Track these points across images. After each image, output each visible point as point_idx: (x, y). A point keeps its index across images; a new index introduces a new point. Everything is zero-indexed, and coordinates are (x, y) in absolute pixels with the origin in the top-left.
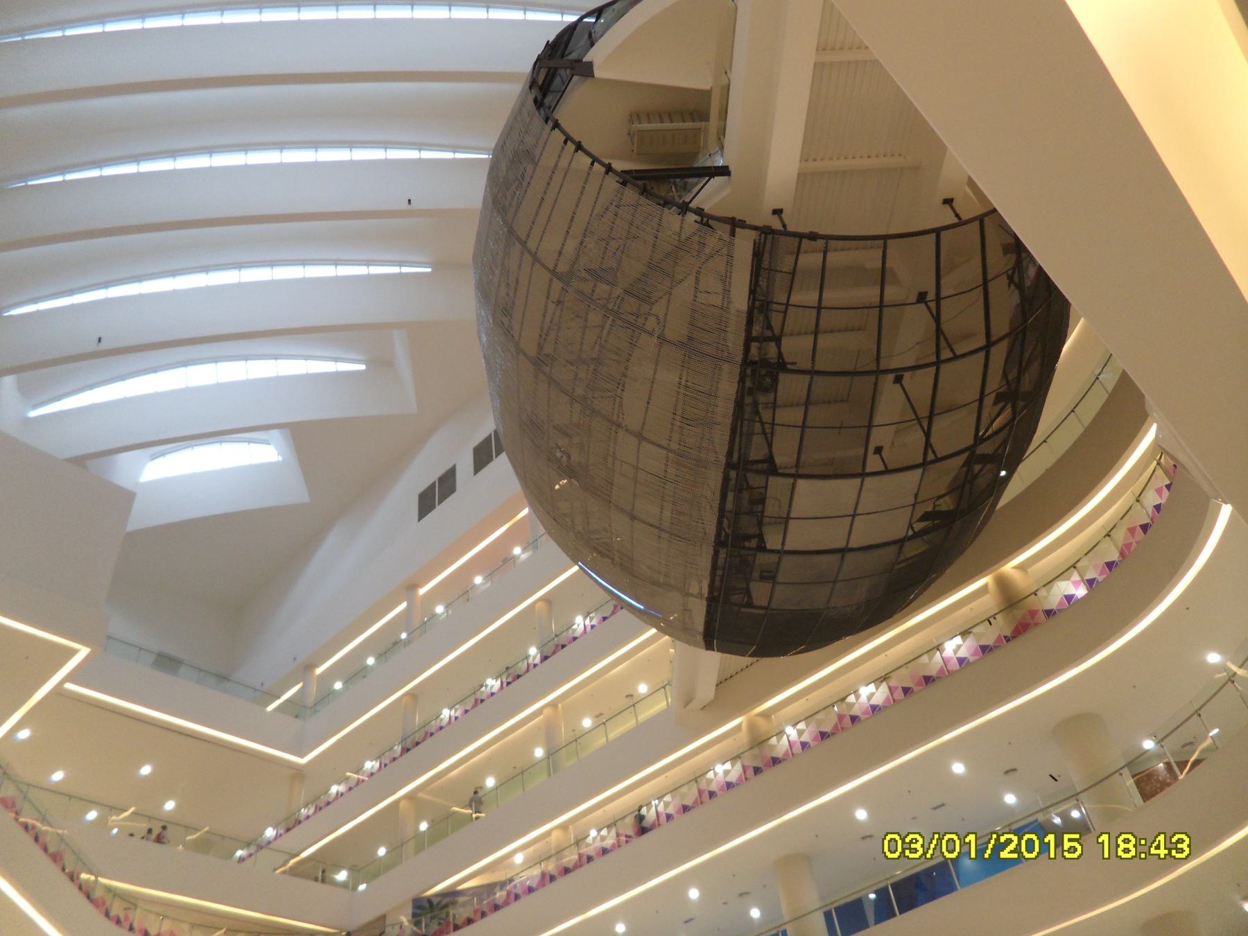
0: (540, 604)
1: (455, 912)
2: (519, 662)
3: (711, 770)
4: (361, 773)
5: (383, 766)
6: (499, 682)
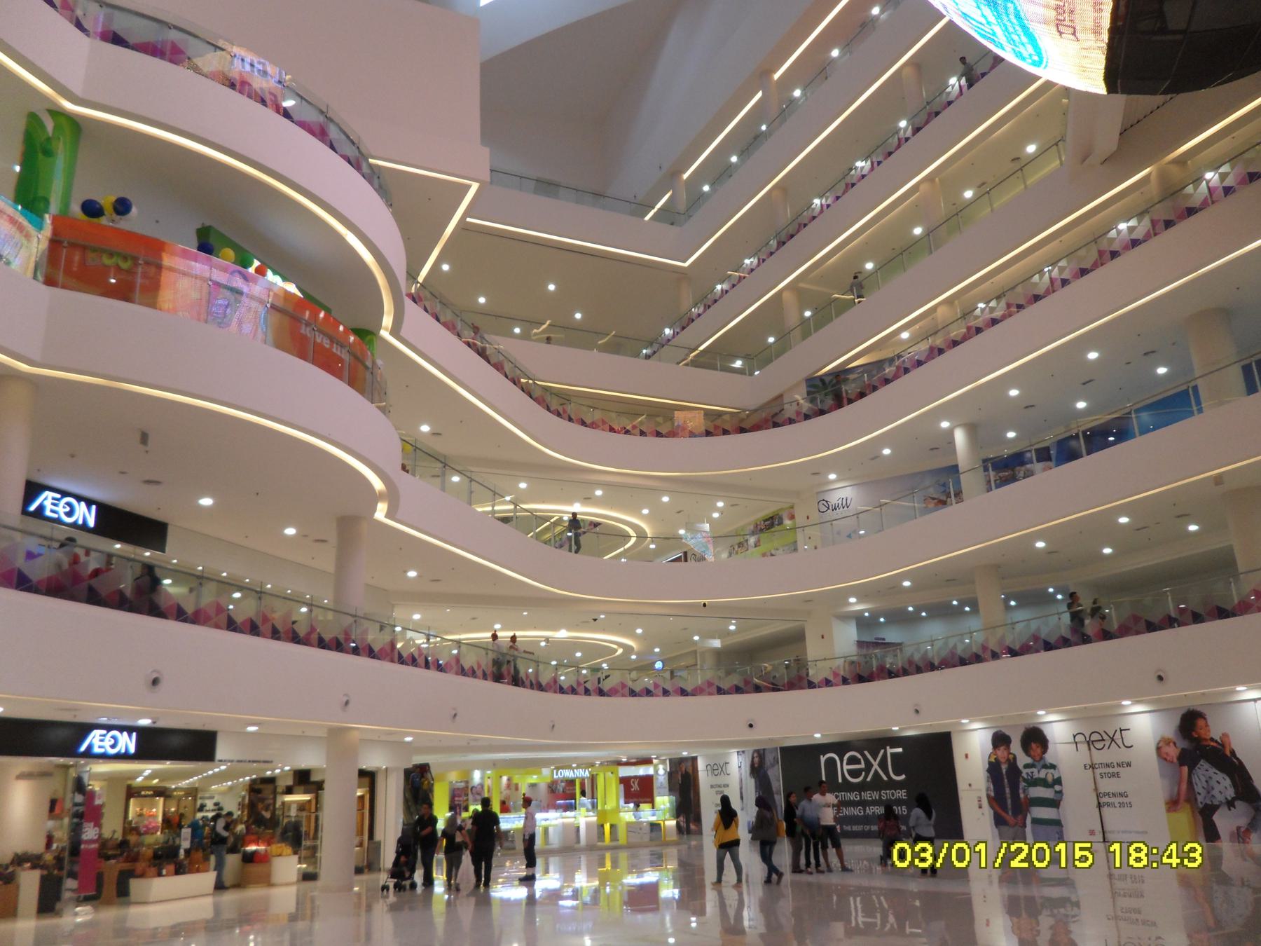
0: (908, 70)
1: (847, 388)
2: (889, 139)
3: (1113, 229)
4: (741, 269)
5: (761, 261)
6: (869, 163)
